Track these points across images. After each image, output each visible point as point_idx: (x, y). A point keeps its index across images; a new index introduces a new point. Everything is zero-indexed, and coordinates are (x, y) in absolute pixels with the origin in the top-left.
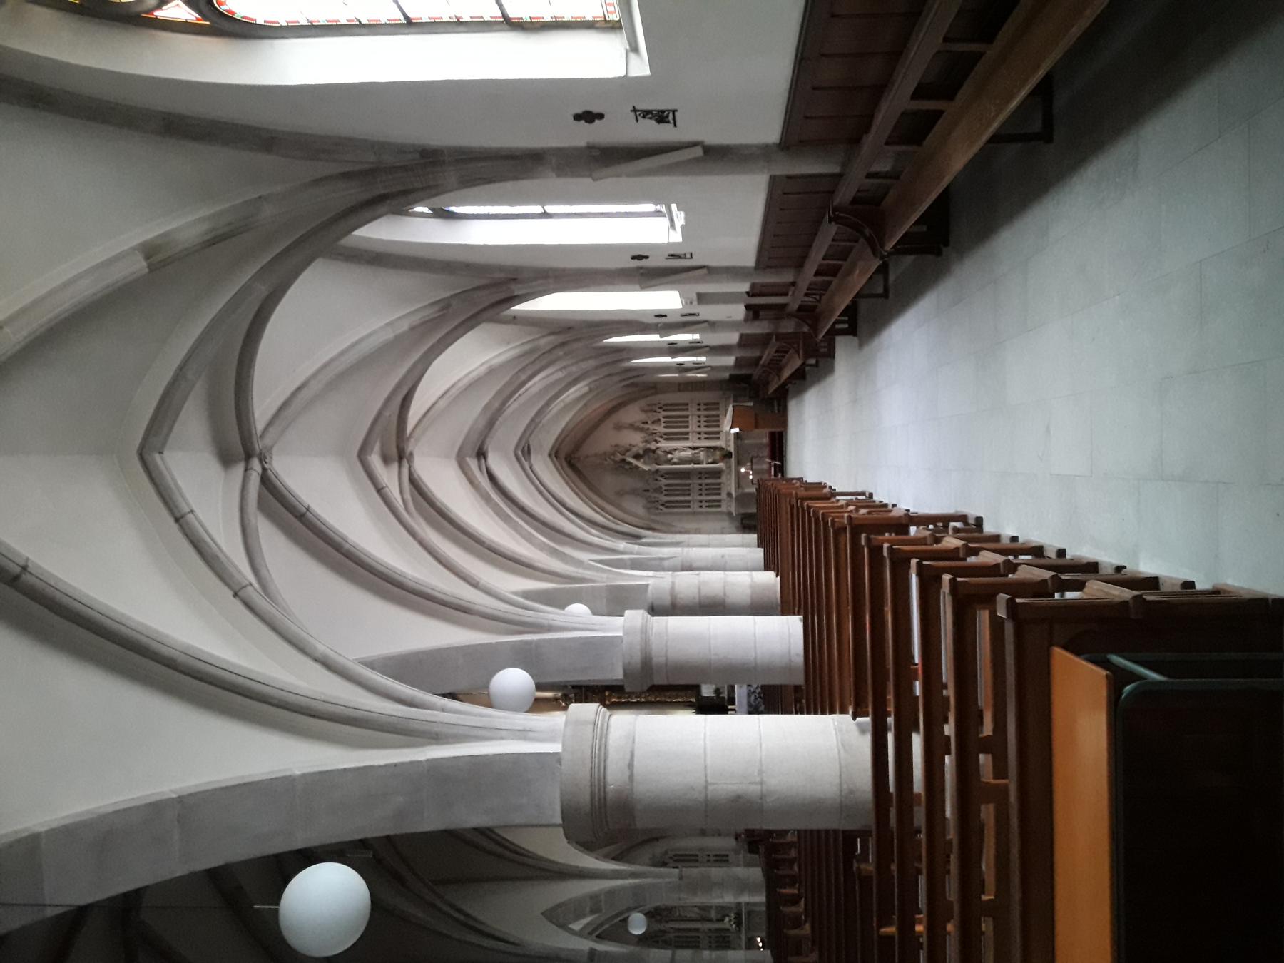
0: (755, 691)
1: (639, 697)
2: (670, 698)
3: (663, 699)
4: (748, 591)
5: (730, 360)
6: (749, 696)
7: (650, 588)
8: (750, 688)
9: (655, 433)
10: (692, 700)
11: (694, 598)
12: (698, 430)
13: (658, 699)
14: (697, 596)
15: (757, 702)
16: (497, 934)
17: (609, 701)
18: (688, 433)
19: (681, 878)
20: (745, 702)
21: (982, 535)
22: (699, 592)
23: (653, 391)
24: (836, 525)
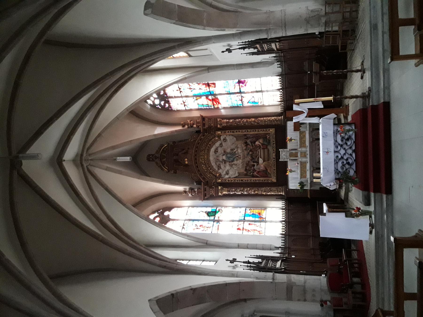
0: (342, 158)
1: (242, 191)
2: (265, 192)
3: (260, 193)
5: (265, 44)
6: (336, 163)
8: (337, 154)
10: (282, 193)
13: (256, 192)
15: (345, 169)
17: (221, 193)
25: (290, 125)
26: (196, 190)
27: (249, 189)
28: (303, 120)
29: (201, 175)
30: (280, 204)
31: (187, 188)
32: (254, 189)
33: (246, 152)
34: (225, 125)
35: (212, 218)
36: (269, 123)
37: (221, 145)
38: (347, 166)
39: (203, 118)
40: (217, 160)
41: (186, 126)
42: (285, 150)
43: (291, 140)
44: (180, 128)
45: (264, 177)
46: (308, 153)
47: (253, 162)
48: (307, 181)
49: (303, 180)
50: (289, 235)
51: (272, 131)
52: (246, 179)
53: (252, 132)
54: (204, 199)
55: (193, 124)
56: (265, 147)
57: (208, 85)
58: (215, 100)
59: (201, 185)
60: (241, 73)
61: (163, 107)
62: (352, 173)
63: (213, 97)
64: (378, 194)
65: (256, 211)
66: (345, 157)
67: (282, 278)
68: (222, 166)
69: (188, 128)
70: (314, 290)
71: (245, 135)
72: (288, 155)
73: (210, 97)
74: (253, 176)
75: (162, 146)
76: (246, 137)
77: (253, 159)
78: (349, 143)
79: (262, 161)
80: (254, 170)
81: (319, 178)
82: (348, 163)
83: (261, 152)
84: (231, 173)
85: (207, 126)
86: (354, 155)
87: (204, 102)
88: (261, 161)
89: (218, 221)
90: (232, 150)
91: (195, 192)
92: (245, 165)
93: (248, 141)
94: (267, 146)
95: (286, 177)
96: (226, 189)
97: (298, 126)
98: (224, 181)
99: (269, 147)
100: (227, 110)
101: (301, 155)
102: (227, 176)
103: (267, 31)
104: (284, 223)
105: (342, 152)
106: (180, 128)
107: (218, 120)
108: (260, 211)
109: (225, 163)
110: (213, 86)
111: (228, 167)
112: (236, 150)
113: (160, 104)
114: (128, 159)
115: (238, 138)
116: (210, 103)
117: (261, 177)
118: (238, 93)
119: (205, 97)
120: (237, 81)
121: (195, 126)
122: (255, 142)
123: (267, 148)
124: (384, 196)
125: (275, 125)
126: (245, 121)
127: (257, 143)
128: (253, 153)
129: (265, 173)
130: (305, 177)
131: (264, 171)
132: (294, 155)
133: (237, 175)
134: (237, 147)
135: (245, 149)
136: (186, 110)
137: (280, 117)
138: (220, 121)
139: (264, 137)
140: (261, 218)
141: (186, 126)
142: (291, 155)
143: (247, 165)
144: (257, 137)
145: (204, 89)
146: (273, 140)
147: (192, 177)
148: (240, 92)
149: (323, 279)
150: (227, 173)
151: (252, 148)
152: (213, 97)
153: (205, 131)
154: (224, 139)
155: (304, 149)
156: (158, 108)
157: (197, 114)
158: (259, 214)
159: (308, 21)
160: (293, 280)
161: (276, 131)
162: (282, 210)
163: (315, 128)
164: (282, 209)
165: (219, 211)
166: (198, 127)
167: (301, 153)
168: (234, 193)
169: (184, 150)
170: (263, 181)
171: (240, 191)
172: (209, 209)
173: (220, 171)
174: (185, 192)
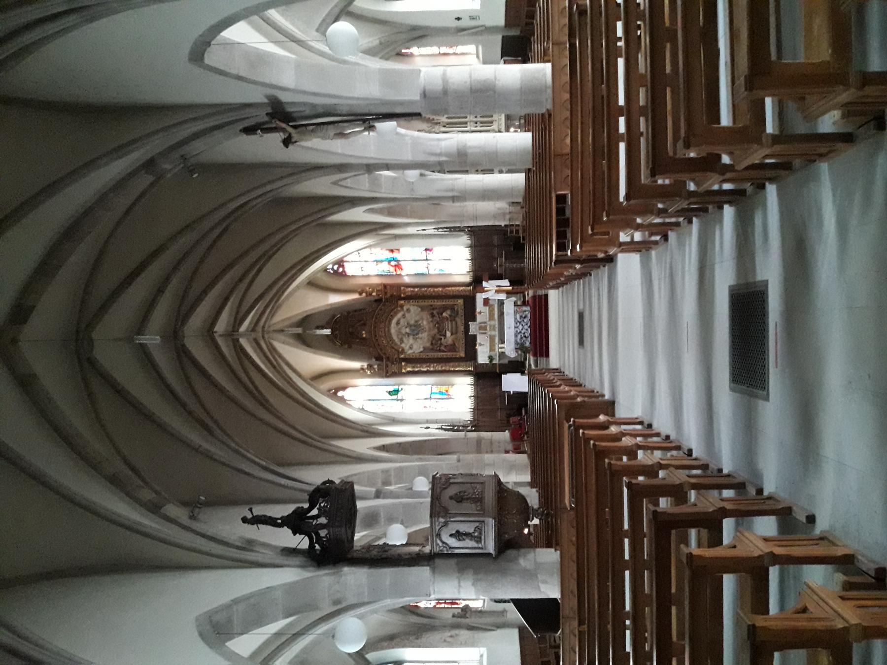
0: (520, 332)
2: (453, 367)
3: (447, 368)
4: (519, 82)
6: (516, 336)
7: (422, 74)
8: (516, 329)
9: (439, 123)
10: (470, 369)
11: (466, 82)
12: (475, 120)
13: (443, 368)
14: (468, 80)
16: (303, 480)
17: (405, 369)
18: (466, 123)
19: (459, 461)
20: (513, 339)
21: (631, 611)
22: (470, 77)
23: (454, 331)
24: (576, 424)
25: (480, 297)
26: (376, 367)
27: (435, 365)
28: (492, 296)
29: (381, 350)
30: (469, 380)
31: (365, 365)
32: (442, 364)
33: (431, 325)
34: (410, 294)
35: (395, 397)
36: (457, 293)
37: (404, 316)
38: (524, 339)
39: (385, 286)
40: (399, 332)
41: (364, 294)
42: (475, 323)
43: (480, 313)
44: (356, 296)
45: (452, 352)
46: (497, 326)
47: (441, 335)
48: (496, 355)
49: (492, 353)
50: (478, 409)
51: (460, 302)
52: (431, 355)
53: (439, 303)
54: (387, 377)
55: (372, 292)
56: (453, 318)
57: (392, 251)
58: (398, 266)
59: (383, 361)
60: (428, 243)
61: (336, 272)
62: (528, 344)
63: (396, 263)
64: (542, 358)
65: (443, 389)
66: (523, 332)
67: (474, 435)
68: (405, 340)
69: (367, 296)
70: (499, 443)
71: (431, 306)
72: (478, 328)
73: (393, 263)
74: (440, 351)
75: (334, 316)
76: (432, 308)
77: (439, 331)
78: (525, 321)
79: (450, 334)
80: (441, 344)
81: (503, 348)
82: (525, 337)
83: (448, 325)
84: (415, 347)
85: (389, 295)
86: (529, 330)
87: (385, 268)
88: (448, 334)
89: (402, 400)
90: (416, 322)
91: (374, 369)
92: (431, 339)
93: (435, 312)
94: (455, 317)
95: (475, 352)
96: (410, 365)
97: (486, 302)
98: (407, 357)
99: (457, 319)
100: (411, 277)
101: (490, 328)
102: (410, 352)
103: (461, 222)
104: (472, 398)
105: (521, 327)
106: (356, 296)
107: (402, 288)
108: (447, 389)
109: (408, 336)
110: (397, 251)
111: (411, 341)
112: (420, 322)
113: (333, 269)
114: (327, 332)
115: (423, 309)
116: (392, 269)
117: (449, 351)
118: (424, 260)
119: (387, 262)
120: (424, 249)
121: (374, 294)
122: (442, 314)
123: (454, 320)
124: (545, 359)
125: (464, 296)
126: (432, 290)
127: (444, 314)
128: (440, 325)
129: (453, 348)
130: (494, 350)
131: (451, 345)
132: (483, 328)
133: (421, 349)
134: (422, 319)
135: (432, 321)
136: (363, 276)
137: (469, 288)
138: (404, 290)
139: (452, 308)
140: (449, 395)
141: (364, 294)
142: (480, 328)
143: (433, 338)
144: (445, 308)
145: (389, 255)
146: (461, 312)
147: (370, 352)
148: (427, 260)
149: (507, 434)
150: (411, 348)
151: (438, 320)
152: (396, 263)
153: (387, 300)
154: (407, 310)
155: (492, 323)
156: (330, 272)
157: (376, 281)
158: (447, 391)
159: (495, 217)
160: (482, 435)
161: (464, 302)
162: (470, 386)
163: (501, 303)
164: (471, 385)
165: (402, 389)
166: (378, 295)
167: (490, 326)
168: (419, 369)
169: (361, 321)
170: (451, 356)
171: (426, 367)
172: (391, 388)
173: (403, 345)
174: (362, 369)
